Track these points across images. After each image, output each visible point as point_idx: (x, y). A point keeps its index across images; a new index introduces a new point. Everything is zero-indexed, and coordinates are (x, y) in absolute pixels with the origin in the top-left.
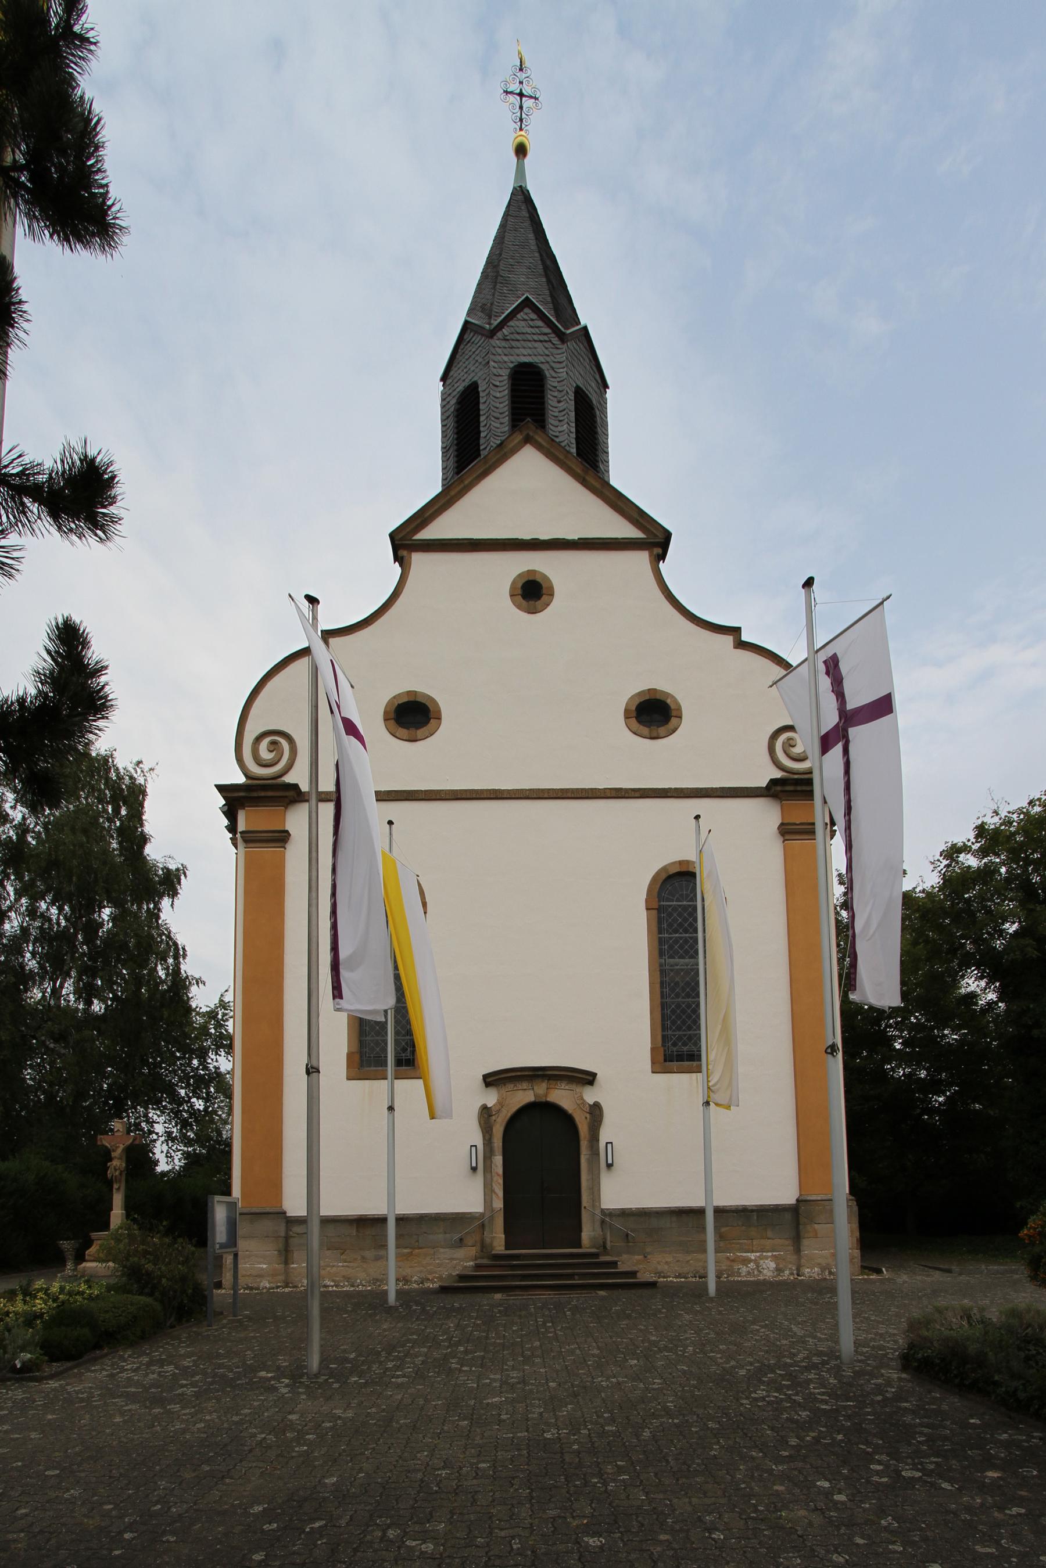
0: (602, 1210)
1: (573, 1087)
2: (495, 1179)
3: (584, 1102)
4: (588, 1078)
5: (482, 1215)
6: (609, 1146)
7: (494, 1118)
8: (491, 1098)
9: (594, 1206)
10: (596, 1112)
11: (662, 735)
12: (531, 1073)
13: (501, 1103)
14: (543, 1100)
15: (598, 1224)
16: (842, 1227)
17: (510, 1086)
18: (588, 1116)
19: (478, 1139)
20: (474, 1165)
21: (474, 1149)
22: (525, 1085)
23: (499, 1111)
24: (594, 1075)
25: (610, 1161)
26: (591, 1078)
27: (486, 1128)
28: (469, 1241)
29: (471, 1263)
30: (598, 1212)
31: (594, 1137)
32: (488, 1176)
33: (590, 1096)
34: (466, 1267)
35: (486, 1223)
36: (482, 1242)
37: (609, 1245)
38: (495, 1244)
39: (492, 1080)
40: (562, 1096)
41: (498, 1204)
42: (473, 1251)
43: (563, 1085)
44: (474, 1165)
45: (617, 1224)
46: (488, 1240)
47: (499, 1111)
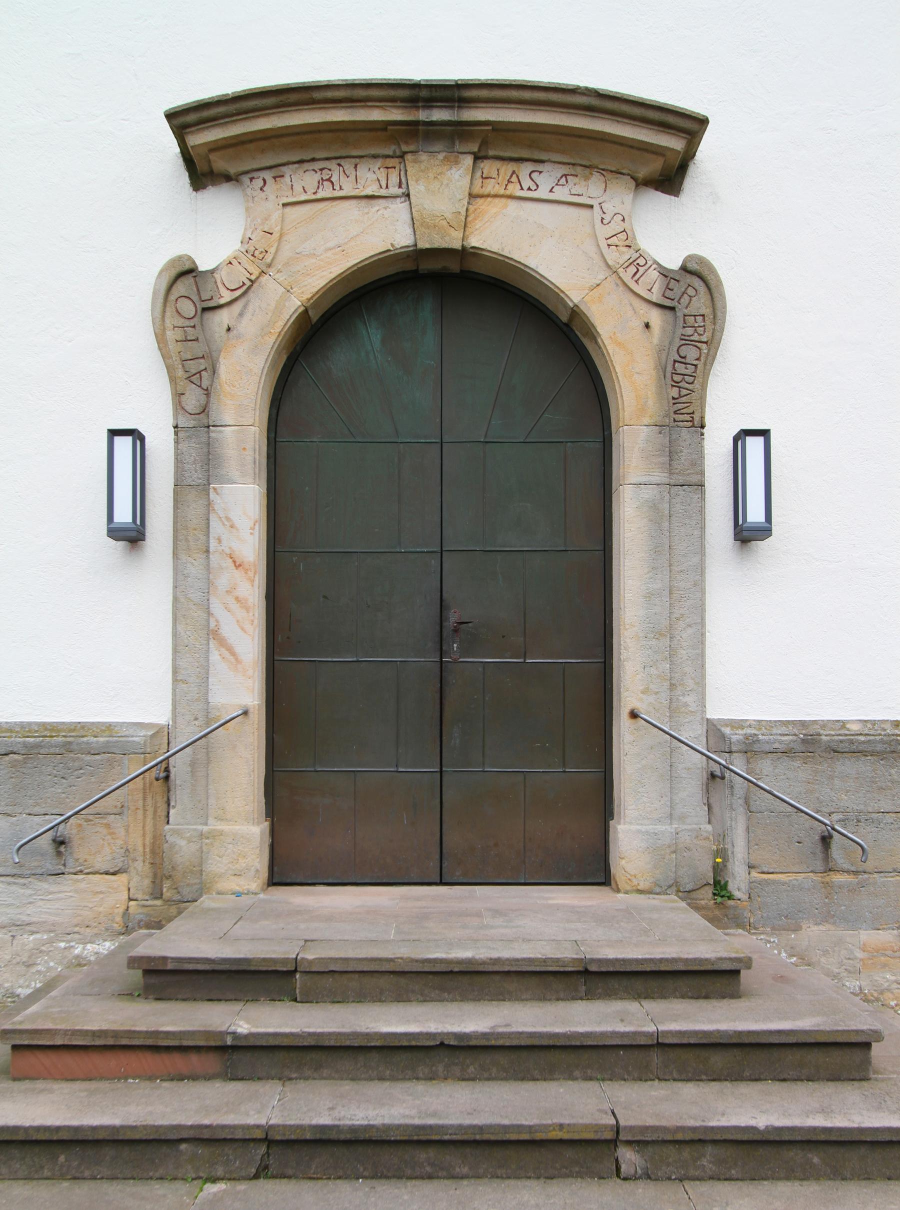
0: (713, 729)
1: (591, 189)
2: (223, 582)
3: (639, 263)
4: (653, 147)
5: (163, 734)
6: (754, 445)
7: (223, 317)
8: (215, 231)
9: (673, 709)
10: (691, 299)
11: (183, 446)
12: (396, 115)
13: (259, 259)
14: (454, 241)
15: (691, 789)
16: (240, 770)
17: (304, 182)
18: (656, 317)
19: (153, 410)
20: (124, 515)
21: (123, 445)
22: (370, 177)
23: (248, 288)
24: (691, 126)
25: (755, 514)
26: (676, 144)
27: (192, 370)
28: (97, 846)
29: (106, 946)
30: (693, 733)
31: (683, 413)
32: (194, 568)
33: (666, 232)
34: (80, 962)
35: (179, 767)
36: (157, 854)
37: (739, 880)
38: (217, 864)
39: (226, 140)
40: (541, 230)
41: (240, 686)
42: (112, 896)
43: (547, 181)
44: (124, 515)
45: (783, 780)
46: (183, 849)
47: (248, 288)
